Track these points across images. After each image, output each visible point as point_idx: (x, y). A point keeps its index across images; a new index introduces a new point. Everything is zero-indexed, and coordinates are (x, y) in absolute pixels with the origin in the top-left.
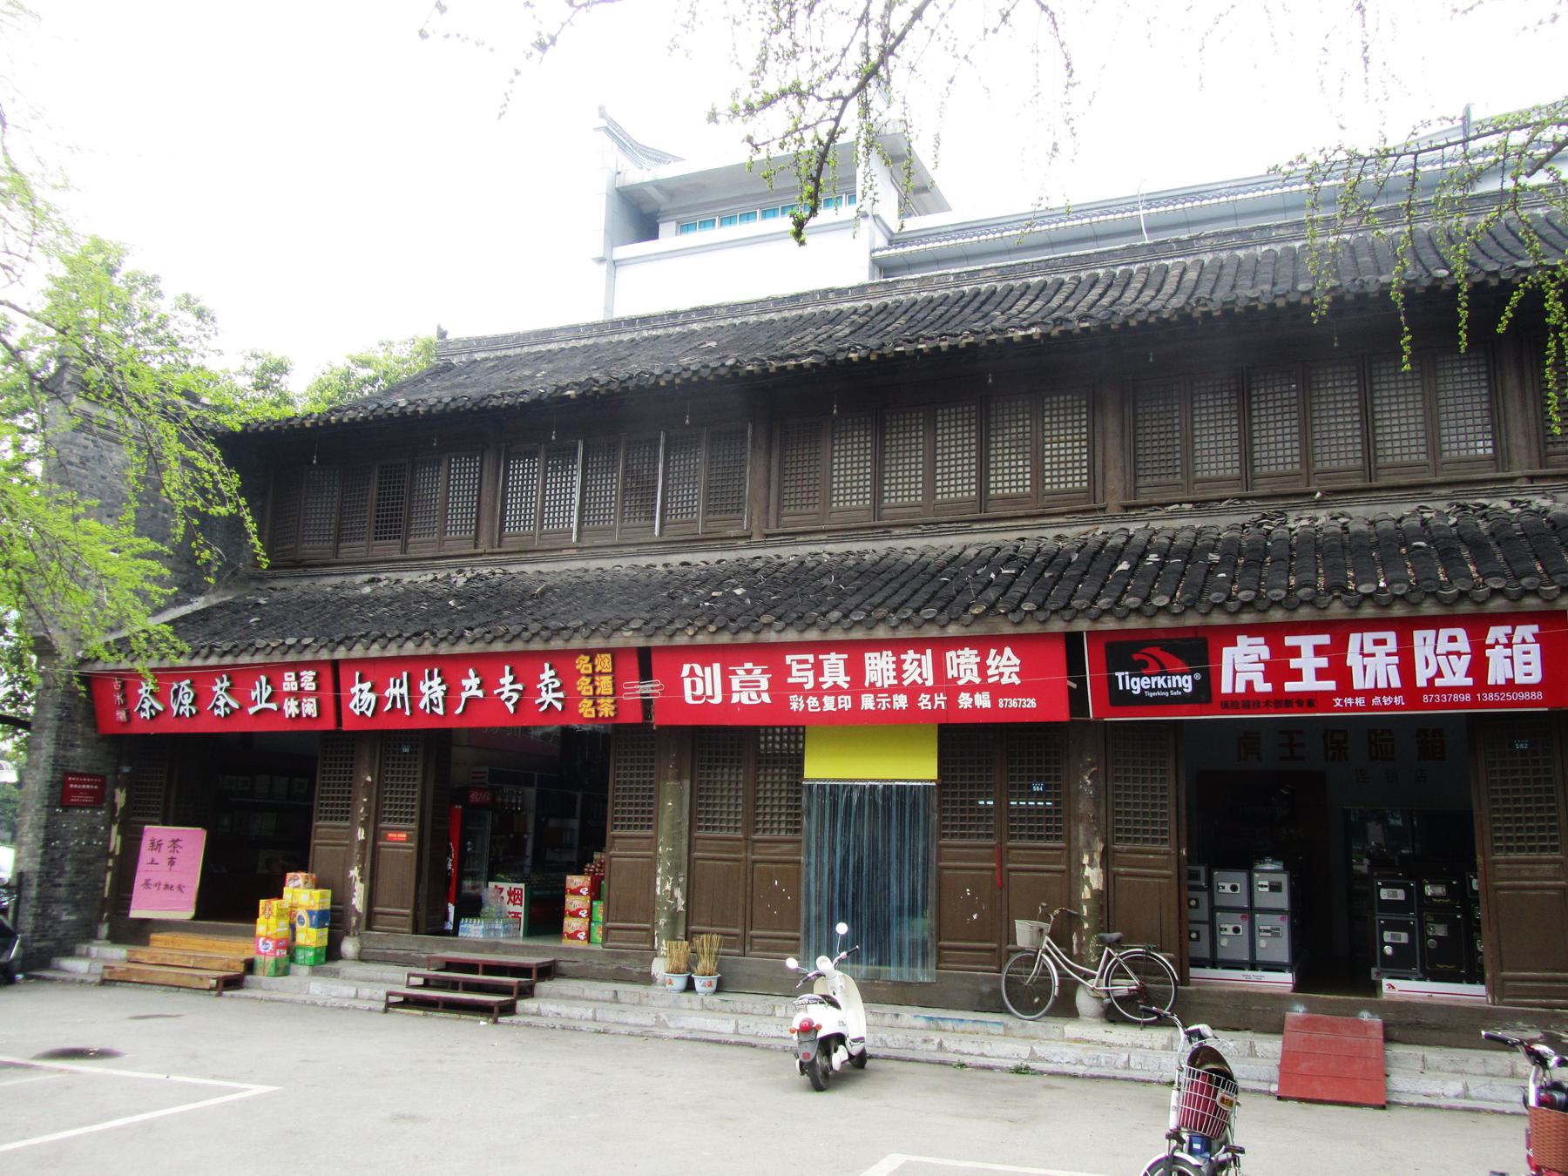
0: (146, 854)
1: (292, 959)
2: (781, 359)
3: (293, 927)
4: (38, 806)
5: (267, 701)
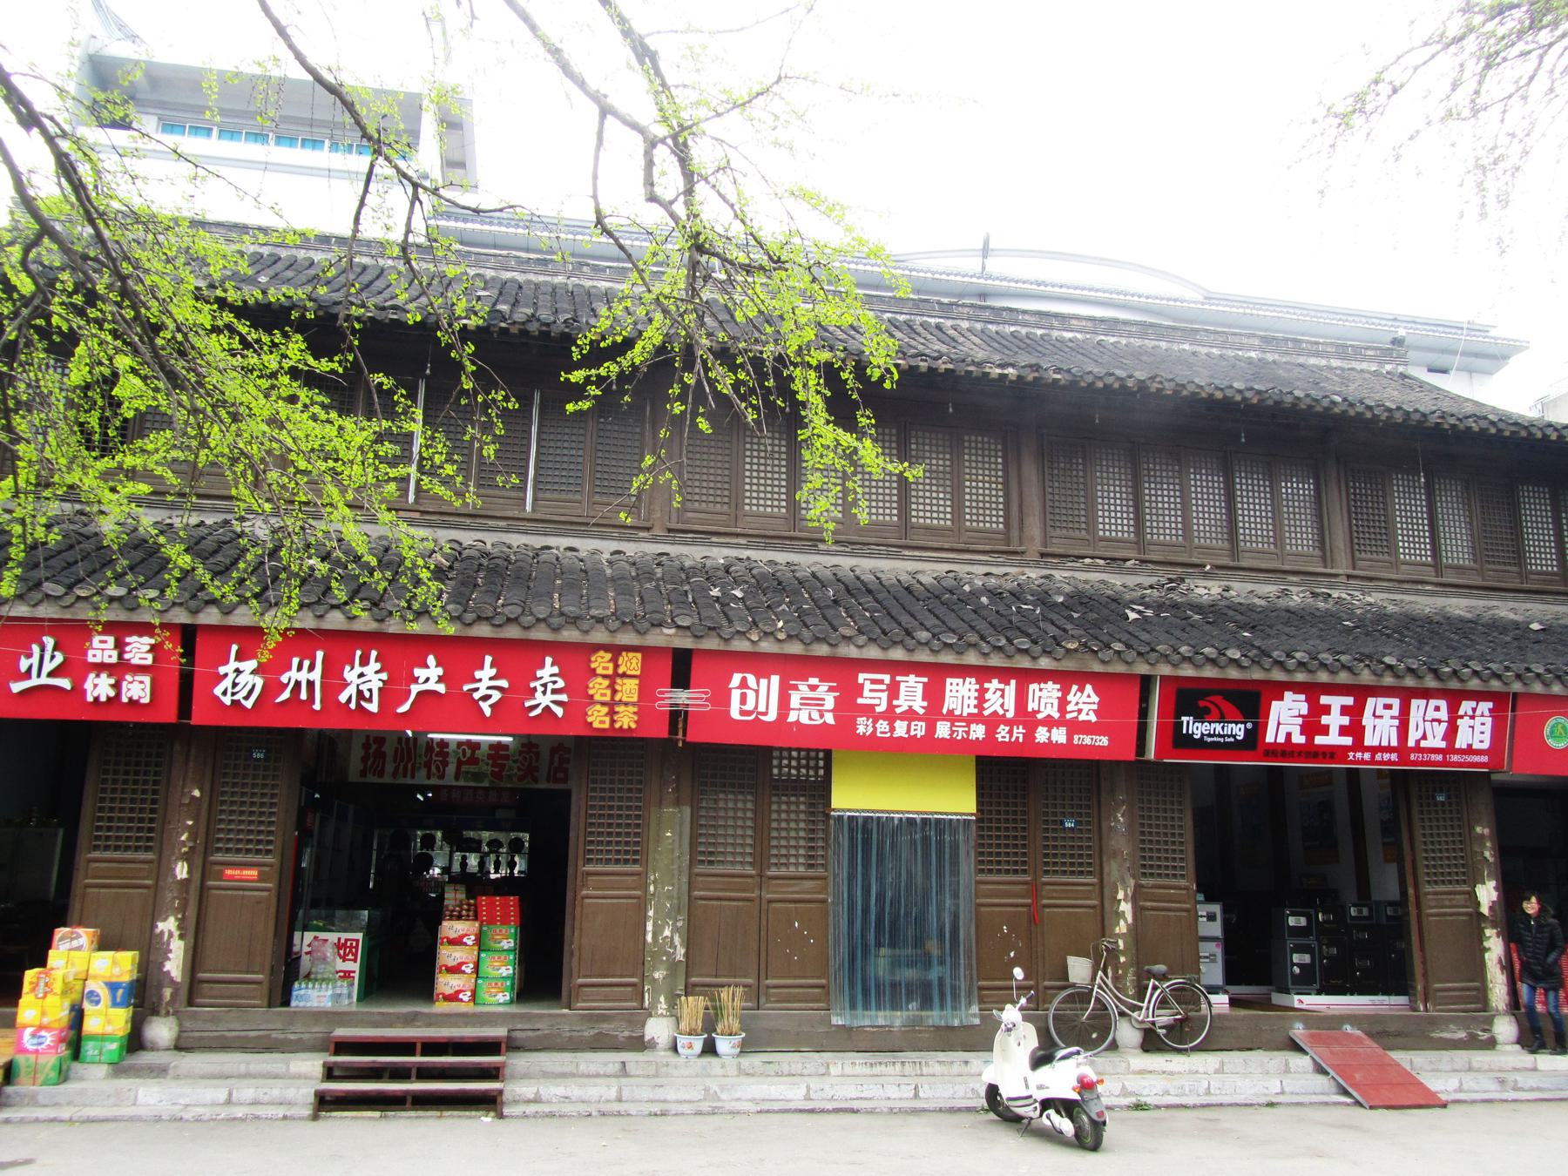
1: (76, 1055)
2: (1002, 366)
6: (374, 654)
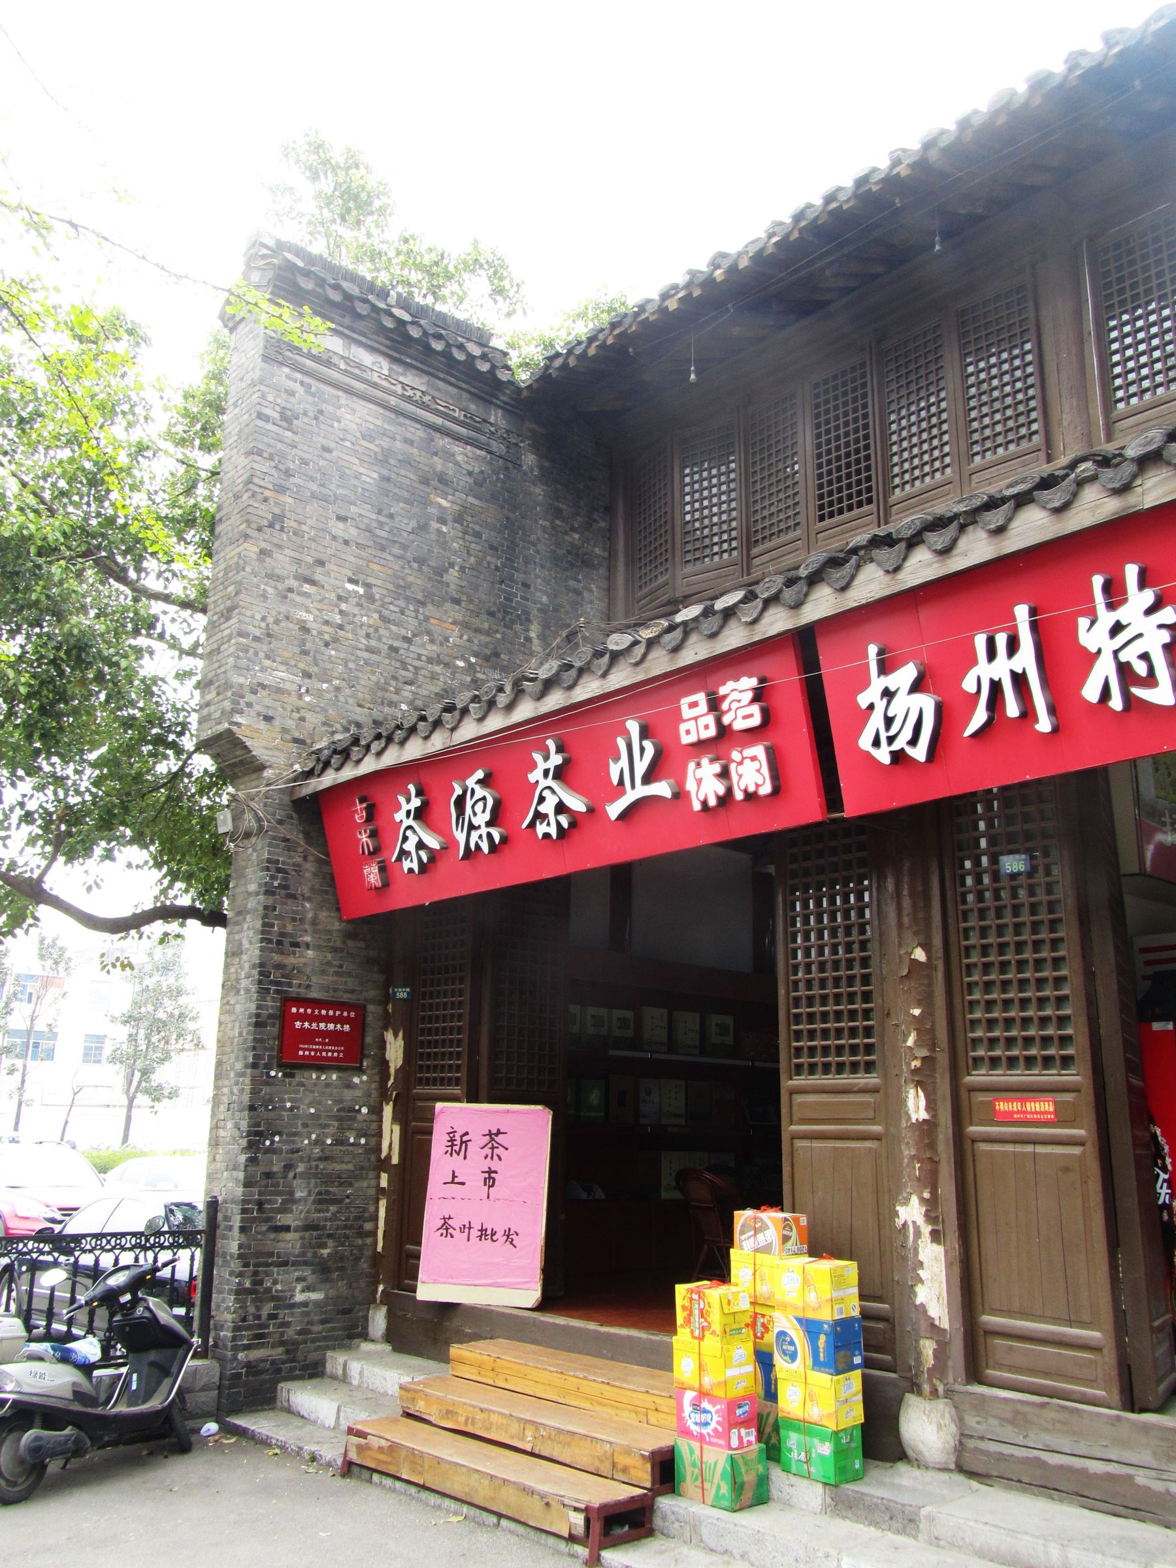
0: (440, 1164)
1: (773, 1452)
3: (764, 1360)
4: (239, 1066)
5: (648, 779)
6: (1131, 572)
